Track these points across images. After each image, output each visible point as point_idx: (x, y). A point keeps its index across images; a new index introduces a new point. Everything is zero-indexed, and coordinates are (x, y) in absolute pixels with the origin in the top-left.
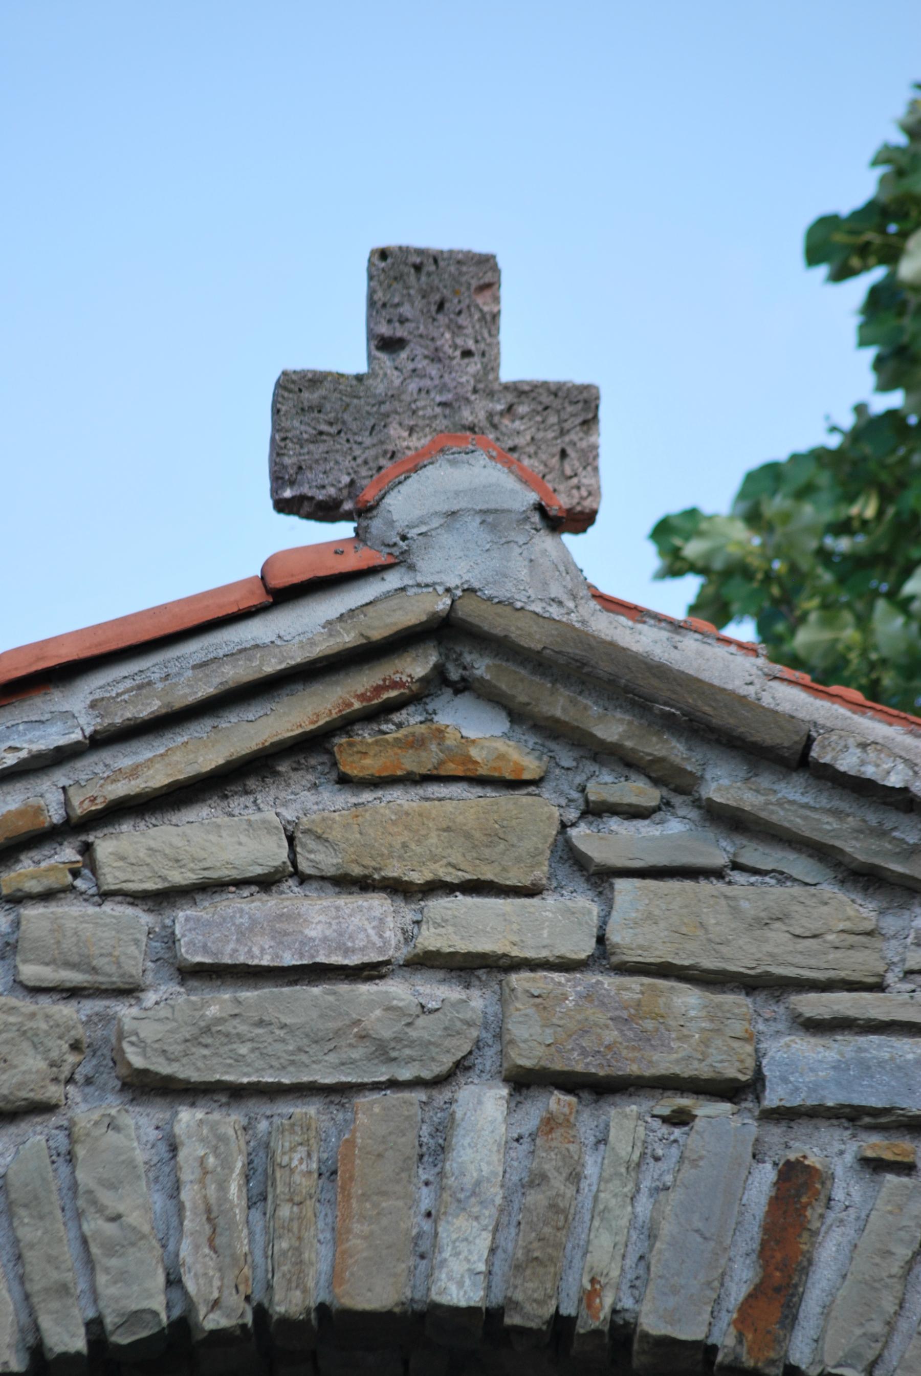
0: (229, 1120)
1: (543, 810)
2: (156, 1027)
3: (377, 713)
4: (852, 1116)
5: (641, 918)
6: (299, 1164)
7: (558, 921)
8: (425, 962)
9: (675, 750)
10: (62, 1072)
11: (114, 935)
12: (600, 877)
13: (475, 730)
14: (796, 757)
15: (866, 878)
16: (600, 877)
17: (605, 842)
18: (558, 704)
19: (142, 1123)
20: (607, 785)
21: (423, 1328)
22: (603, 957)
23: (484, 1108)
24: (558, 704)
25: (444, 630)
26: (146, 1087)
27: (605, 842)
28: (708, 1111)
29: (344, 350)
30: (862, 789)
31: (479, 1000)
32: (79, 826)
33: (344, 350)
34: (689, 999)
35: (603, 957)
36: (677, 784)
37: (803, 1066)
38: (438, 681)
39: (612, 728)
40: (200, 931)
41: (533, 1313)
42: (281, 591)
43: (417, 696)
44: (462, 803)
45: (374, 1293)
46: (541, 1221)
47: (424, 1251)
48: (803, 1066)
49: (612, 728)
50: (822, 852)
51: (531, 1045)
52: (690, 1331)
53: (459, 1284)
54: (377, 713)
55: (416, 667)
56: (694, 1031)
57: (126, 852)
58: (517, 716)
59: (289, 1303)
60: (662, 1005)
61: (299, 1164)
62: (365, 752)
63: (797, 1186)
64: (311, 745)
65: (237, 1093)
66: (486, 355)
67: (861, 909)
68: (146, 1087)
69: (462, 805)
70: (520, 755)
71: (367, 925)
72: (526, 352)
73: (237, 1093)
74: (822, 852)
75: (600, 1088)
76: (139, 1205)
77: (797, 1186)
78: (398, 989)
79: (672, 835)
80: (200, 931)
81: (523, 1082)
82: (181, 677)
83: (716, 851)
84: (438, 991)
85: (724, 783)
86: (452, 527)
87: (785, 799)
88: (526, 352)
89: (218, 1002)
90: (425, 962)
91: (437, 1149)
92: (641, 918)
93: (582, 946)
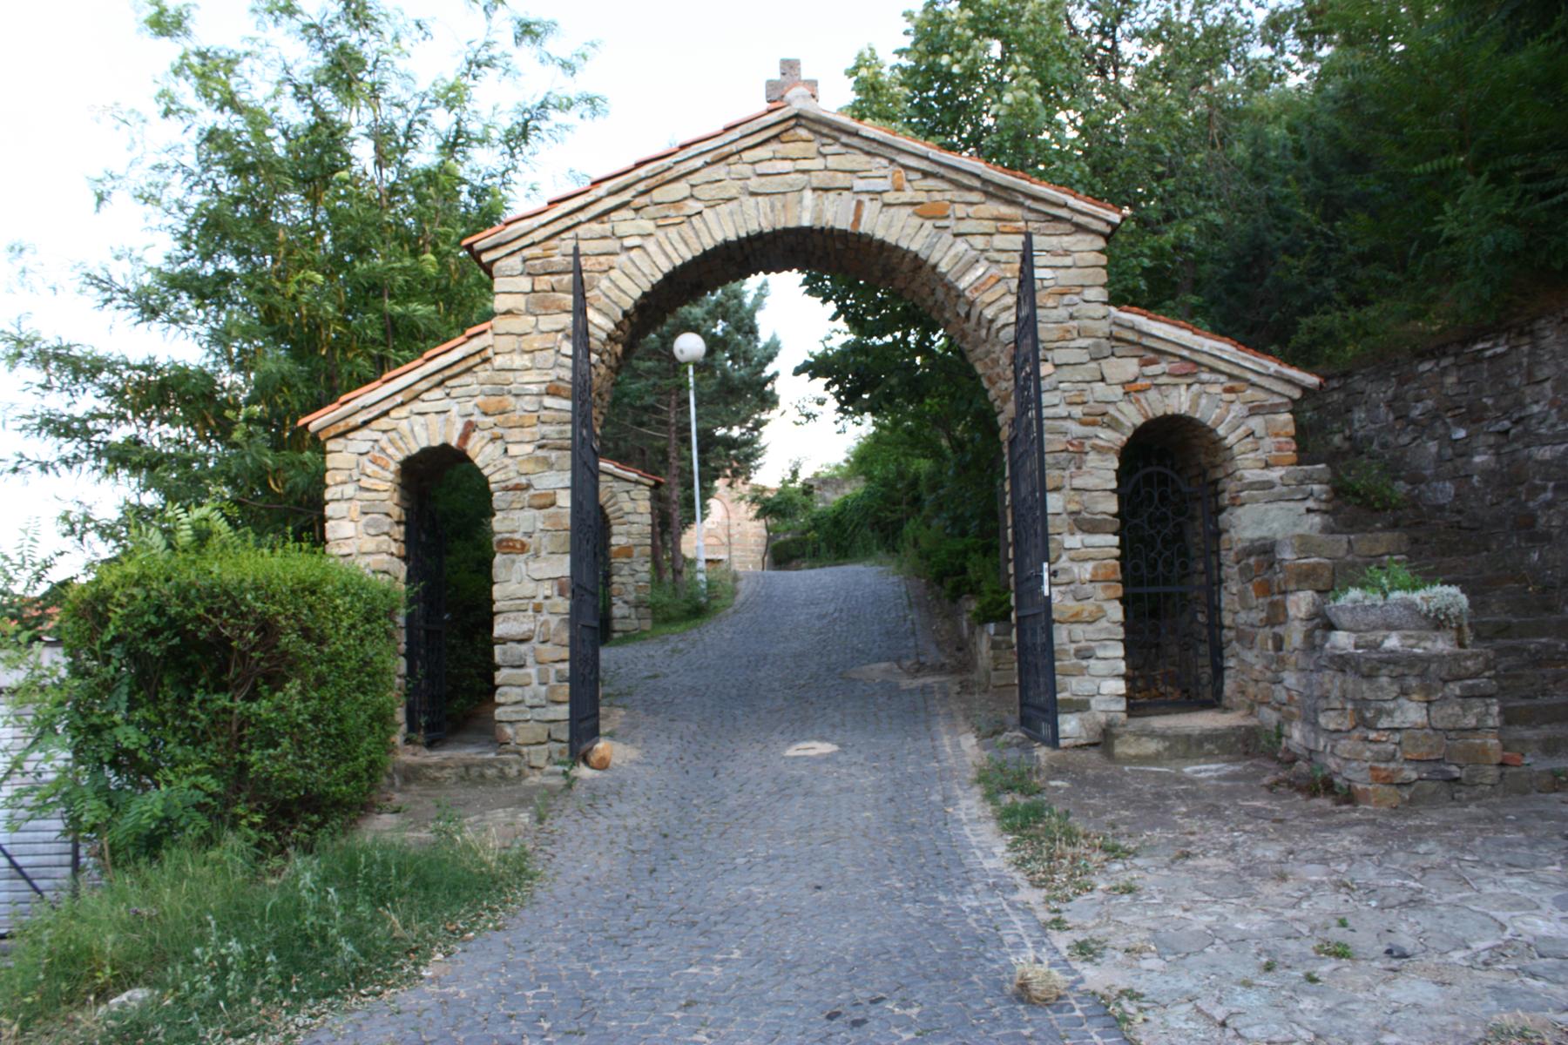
0: (767, 198)
1: (815, 145)
2: (754, 184)
3: (786, 130)
4: (868, 192)
5: (832, 162)
6: (778, 205)
7: (818, 163)
8: (797, 171)
9: (836, 134)
10: (231, 455)
11: (746, 170)
12: (825, 156)
13: (803, 133)
14: (856, 134)
15: (868, 153)
16: (825, 156)
17: (825, 150)
18: (816, 127)
19: (752, 200)
20: (826, 141)
21: (800, 231)
22: (826, 169)
23: (808, 194)
24: (816, 127)
25: (797, 116)
26: (753, 194)
27: (825, 150)
28: (845, 193)
29: (777, 76)
30: (867, 138)
31: (805, 177)
32: (739, 152)
33: (777, 76)
34: (840, 175)
35: (826, 169)
36: (836, 140)
37: (859, 185)
38: (797, 125)
39: (825, 130)
40: (760, 168)
41: (818, 226)
42: (770, 111)
43: (793, 128)
44: (801, 144)
45: (792, 224)
46: (819, 212)
47: (800, 218)
48: (859, 185)
49: (825, 130)
50: (861, 149)
51: (815, 184)
52: (843, 227)
53: (806, 222)
54: (786, 130)
55: (792, 122)
56: (842, 180)
57: (747, 156)
58: (810, 130)
59: (778, 227)
60: (238, 378)
61: (778, 205)
62: (785, 137)
63: (860, 203)
64: (776, 137)
65: (767, 194)
66: (798, 74)
67: (867, 158)
68: (753, 194)
69: (801, 145)
70: (810, 136)
71: (788, 166)
72: (805, 75)
73: (767, 194)
74: (861, 149)
75: (827, 190)
76: (753, 212)
77: (860, 203)
78: (793, 176)
79: (836, 148)
80: (760, 168)
81: (814, 190)
82: (755, 126)
83: (843, 150)
84: (799, 176)
85: (844, 139)
86: (797, 101)
87: (855, 141)
88: (805, 75)
89: (763, 179)
90: (797, 171)
91: (800, 201)
92: (832, 162)
93: (528, 288)
